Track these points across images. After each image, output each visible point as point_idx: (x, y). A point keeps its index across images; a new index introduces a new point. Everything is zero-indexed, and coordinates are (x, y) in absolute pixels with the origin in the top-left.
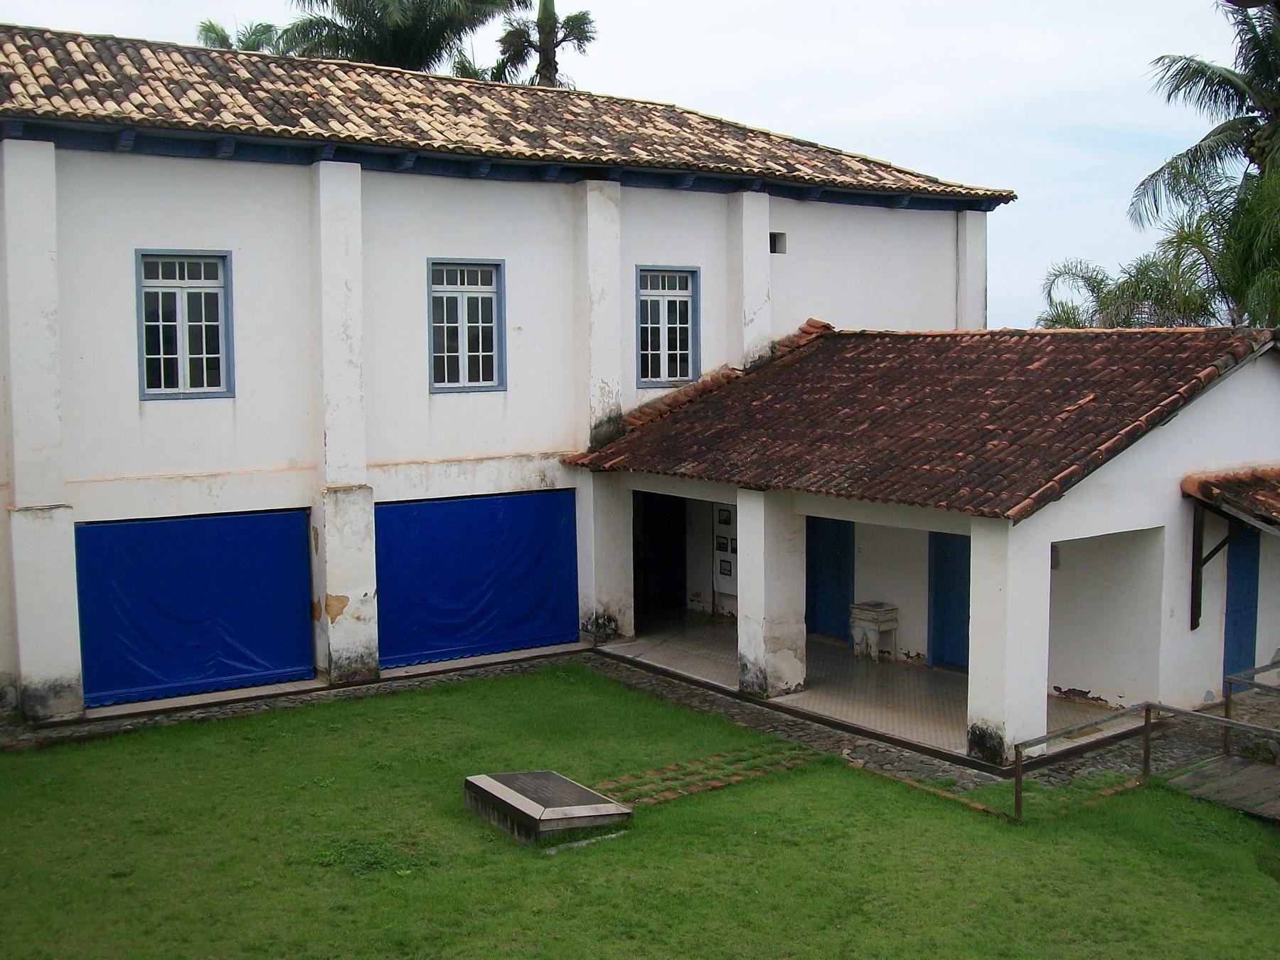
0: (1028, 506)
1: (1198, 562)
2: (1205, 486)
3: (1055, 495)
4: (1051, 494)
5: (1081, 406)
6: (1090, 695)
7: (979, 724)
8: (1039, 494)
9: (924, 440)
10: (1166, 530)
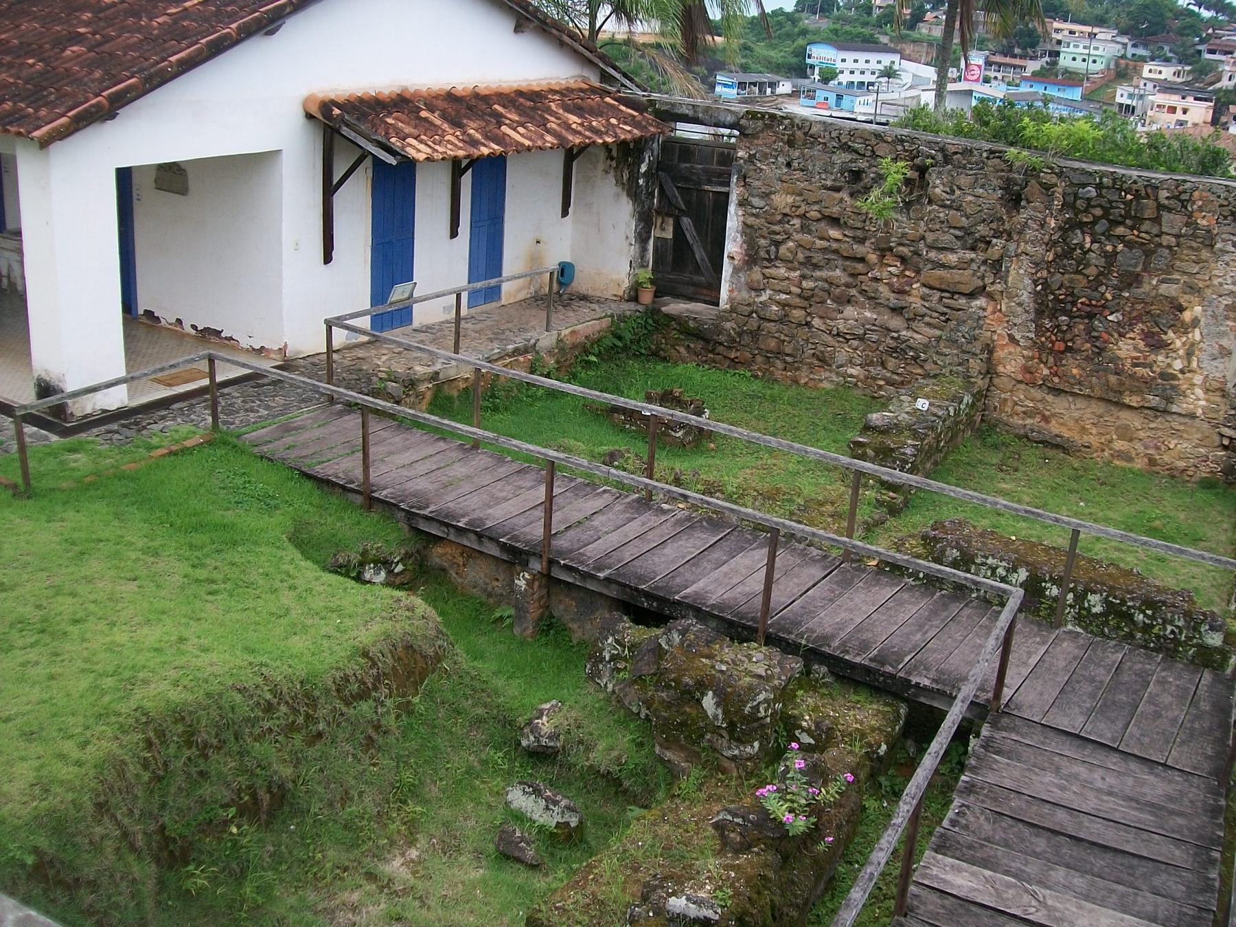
0: (62, 126)
1: (329, 189)
2: (327, 106)
3: (107, 113)
4: (97, 112)
5: (186, 9)
6: (223, 335)
7: (44, 376)
8: (79, 113)
9: (8, 42)
10: (285, 156)
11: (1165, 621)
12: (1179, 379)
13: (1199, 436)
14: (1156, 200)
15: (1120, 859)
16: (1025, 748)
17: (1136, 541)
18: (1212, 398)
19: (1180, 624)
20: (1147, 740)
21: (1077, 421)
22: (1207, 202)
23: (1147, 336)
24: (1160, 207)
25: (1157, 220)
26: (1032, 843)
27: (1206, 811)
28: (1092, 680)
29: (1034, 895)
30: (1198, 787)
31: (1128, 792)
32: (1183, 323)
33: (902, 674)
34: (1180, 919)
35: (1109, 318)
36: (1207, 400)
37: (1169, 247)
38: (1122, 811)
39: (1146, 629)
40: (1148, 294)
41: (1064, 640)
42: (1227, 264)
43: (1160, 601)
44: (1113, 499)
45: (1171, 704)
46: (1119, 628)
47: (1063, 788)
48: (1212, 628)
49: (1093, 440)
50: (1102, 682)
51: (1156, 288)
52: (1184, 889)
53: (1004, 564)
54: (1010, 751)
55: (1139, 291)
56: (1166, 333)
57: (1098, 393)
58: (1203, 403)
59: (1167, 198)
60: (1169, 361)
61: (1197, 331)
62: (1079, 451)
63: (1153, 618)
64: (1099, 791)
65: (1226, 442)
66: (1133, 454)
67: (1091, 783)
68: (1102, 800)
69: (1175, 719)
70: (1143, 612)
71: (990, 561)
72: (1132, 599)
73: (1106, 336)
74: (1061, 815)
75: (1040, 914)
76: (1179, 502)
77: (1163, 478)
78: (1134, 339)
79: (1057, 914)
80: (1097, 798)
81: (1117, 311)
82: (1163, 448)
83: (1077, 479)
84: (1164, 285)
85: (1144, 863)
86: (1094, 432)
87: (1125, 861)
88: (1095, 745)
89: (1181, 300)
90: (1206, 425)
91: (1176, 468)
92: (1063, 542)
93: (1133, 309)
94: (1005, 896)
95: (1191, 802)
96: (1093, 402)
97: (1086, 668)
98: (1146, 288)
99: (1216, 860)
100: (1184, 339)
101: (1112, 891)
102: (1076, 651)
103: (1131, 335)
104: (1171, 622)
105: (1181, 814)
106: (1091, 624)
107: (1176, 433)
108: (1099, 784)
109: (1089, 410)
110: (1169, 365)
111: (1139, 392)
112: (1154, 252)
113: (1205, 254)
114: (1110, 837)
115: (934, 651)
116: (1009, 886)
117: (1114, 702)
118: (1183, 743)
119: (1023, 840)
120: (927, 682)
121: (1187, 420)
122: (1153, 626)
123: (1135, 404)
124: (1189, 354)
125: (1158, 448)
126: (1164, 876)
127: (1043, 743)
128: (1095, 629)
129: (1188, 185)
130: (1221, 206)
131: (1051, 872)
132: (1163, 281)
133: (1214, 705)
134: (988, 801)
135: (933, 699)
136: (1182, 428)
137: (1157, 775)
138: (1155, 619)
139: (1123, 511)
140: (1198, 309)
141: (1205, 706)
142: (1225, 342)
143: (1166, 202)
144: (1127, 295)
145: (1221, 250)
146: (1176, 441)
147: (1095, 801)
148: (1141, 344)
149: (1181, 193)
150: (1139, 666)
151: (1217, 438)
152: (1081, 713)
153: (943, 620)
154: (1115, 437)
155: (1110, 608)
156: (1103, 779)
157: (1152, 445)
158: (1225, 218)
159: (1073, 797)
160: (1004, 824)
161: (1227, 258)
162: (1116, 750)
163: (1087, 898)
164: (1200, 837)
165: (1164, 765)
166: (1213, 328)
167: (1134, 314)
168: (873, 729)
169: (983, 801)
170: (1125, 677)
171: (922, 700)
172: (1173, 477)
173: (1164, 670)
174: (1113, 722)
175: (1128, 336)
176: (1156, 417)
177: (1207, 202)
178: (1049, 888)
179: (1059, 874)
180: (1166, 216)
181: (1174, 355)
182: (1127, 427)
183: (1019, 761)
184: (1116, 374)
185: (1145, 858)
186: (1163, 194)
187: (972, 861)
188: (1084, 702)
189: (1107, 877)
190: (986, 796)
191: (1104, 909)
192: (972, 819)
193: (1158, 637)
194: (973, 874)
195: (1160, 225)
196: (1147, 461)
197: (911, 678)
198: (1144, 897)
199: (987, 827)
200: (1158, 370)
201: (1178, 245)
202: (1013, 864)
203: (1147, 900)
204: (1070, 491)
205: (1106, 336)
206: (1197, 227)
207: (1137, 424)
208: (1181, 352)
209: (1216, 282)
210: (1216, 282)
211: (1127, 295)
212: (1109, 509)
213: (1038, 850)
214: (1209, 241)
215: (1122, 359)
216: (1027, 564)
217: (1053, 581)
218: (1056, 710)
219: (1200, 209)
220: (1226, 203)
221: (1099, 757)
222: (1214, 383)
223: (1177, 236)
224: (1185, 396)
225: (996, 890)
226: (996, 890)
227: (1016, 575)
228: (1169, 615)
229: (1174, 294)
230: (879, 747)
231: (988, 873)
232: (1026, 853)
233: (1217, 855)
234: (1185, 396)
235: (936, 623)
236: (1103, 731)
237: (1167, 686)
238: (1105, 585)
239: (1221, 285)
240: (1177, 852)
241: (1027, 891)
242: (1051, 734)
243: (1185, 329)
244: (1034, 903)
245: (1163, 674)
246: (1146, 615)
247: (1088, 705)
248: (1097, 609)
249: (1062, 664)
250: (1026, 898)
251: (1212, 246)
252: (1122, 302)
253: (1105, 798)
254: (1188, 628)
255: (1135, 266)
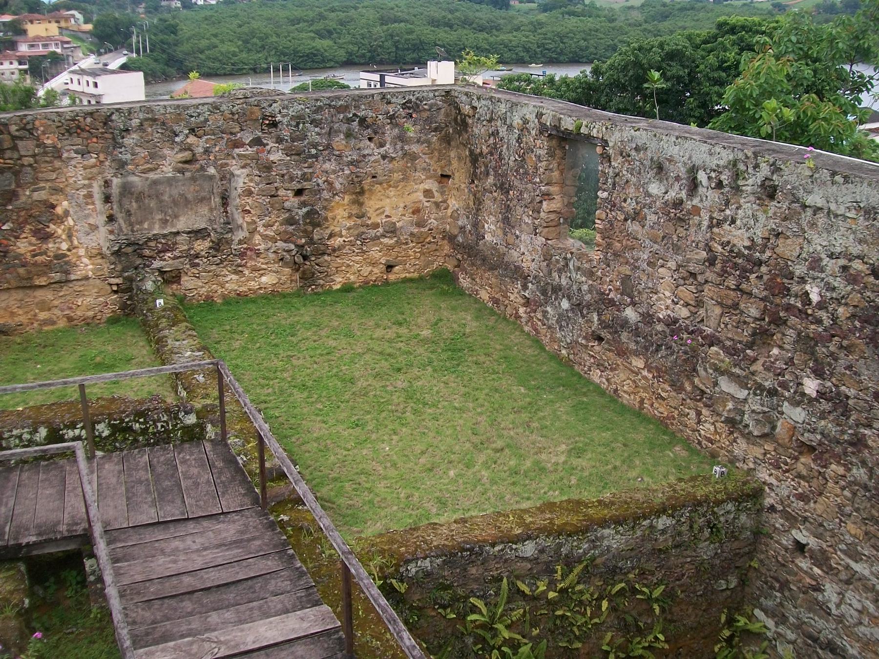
11: (155, 422)
12: (68, 256)
13: (96, 290)
14: (9, 133)
15: (241, 587)
16: (131, 549)
17: (126, 376)
18: (96, 262)
19: (165, 419)
20: (202, 503)
21: (5, 309)
22: (47, 127)
23: (36, 233)
24: (14, 138)
25: (15, 148)
26: (182, 608)
27: (267, 528)
28: (140, 482)
29: (209, 640)
30: (252, 516)
31: (216, 542)
32: (58, 217)
33: (12, 542)
34: (301, 602)
35: (3, 228)
36: (93, 264)
37: (30, 165)
38: (222, 556)
39: (144, 432)
40: (25, 203)
41: (104, 464)
42: (75, 167)
43: (145, 410)
44: (57, 354)
45: (199, 473)
46: (126, 439)
47: (175, 562)
48: (187, 413)
49: (23, 319)
50: (147, 480)
51: (30, 197)
52: (289, 583)
53: (26, 430)
54: (125, 556)
55: (18, 202)
56: (48, 227)
57: (14, 284)
58: (91, 267)
59: (17, 130)
60: (57, 245)
61: (70, 219)
62: (16, 330)
63: (145, 422)
64: (198, 550)
65: (115, 288)
66: (55, 318)
67: (189, 549)
68: (203, 556)
69: (208, 481)
70: (138, 421)
71: (15, 432)
72: (127, 416)
73: (5, 242)
74: (187, 579)
75: (222, 650)
76: (102, 339)
77: (82, 327)
78: (26, 238)
79: (232, 643)
80: (199, 556)
81: (8, 221)
82: (74, 306)
83: (25, 350)
84: (36, 193)
85: (255, 581)
86: (21, 312)
87: (244, 586)
88: (151, 528)
89: (51, 201)
90: (98, 281)
91: (88, 318)
92: (76, 396)
93: (19, 216)
94: (193, 652)
95: (254, 527)
96: (13, 292)
97: (130, 475)
98: (23, 199)
99: (293, 555)
100: (63, 227)
101: (251, 609)
102: (117, 467)
103: (24, 235)
104: (159, 420)
105: (254, 539)
106: (105, 445)
107: (80, 294)
108: (195, 547)
109: (12, 298)
110: (59, 249)
111: (45, 274)
112: (20, 172)
113: (57, 164)
114: (225, 576)
115: (23, 514)
116: (191, 644)
117: (164, 490)
118: (223, 493)
119: (175, 609)
120: (34, 539)
121: (84, 282)
122: (148, 428)
123: (44, 284)
124: (70, 236)
125: (71, 308)
126: (273, 582)
127: (141, 539)
128: (109, 447)
129: (29, 118)
130: (58, 127)
131: (209, 619)
132: (34, 191)
133: (224, 461)
134: (135, 597)
135: (44, 547)
136: (82, 288)
137: (224, 522)
138: (148, 423)
139: (69, 361)
140: (65, 203)
141: (220, 464)
142: (91, 221)
143: (17, 133)
144: (10, 207)
145: (68, 158)
146: (81, 299)
147: (200, 558)
148: (33, 240)
149: (25, 125)
150: (162, 459)
151: (108, 287)
152: (150, 506)
153: (13, 489)
154: (37, 311)
155: (115, 429)
156: (194, 542)
157: (65, 307)
158: (63, 135)
159: (185, 564)
160: (156, 607)
161: (73, 162)
162: (188, 519)
163: (241, 622)
164: (275, 546)
165: (223, 513)
166: (80, 213)
167: (21, 219)
168: (11, 593)
169: (132, 599)
170: (159, 470)
171: (35, 553)
172: (88, 324)
173: (179, 453)
174: (173, 502)
175: (22, 236)
176: (62, 287)
177: (47, 127)
178: (215, 630)
179: (214, 618)
180: (20, 144)
181: (59, 240)
182: (43, 302)
183: (134, 559)
184: (23, 266)
185: (254, 577)
186: (13, 128)
187: (156, 642)
188: (146, 498)
189: (242, 602)
190: (131, 594)
191: (256, 623)
192: (134, 615)
193: (154, 434)
194: (163, 650)
195: (18, 151)
196: (65, 319)
197: (20, 541)
198: (272, 601)
199: (147, 614)
200: (51, 254)
201: (36, 162)
202: (182, 629)
203: (275, 602)
204: (26, 361)
205: (5, 242)
206: (45, 146)
207: (50, 297)
208: (64, 237)
209: (71, 181)
210: (71, 181)
211: (10, 207)
212: (59, 362)
213: (189, 610)
214: (57, 154)
215: (22, 255)
216: (43, 423)
217: (67, 427)
218: (132, 513)
219: (44, 133)
220: (60, 124)
221: (181, 530)
222: (93, 251)
223: (34, 156)
224: (77, 266)
225: (185, 651)
226: (185, 651)
227: (38, 435)
228: (156, 416)
229: (45, 197)
230: (23, 603)
231: (171, 644)
232: (183, 617)
233: (291, 552)
234: (77, 266)
235: (9, 493)
236: (172, 511)
237: (189, 463)
238: (103, 414)
239: (75, 182)
240: (269, 563)
241: (203, 640)
242: (142, 530)
243: (59, 220)
244: (214, 645)
245: (181, 456)
246: (140, 423)
247: (150, 499)
248: (106, 433)
249: (114, 480)
250: (207, 645)
251: (60, 157)
252: (9, 214)
253: (205, 553)
254: (171, 419)
255: (10, 185)
